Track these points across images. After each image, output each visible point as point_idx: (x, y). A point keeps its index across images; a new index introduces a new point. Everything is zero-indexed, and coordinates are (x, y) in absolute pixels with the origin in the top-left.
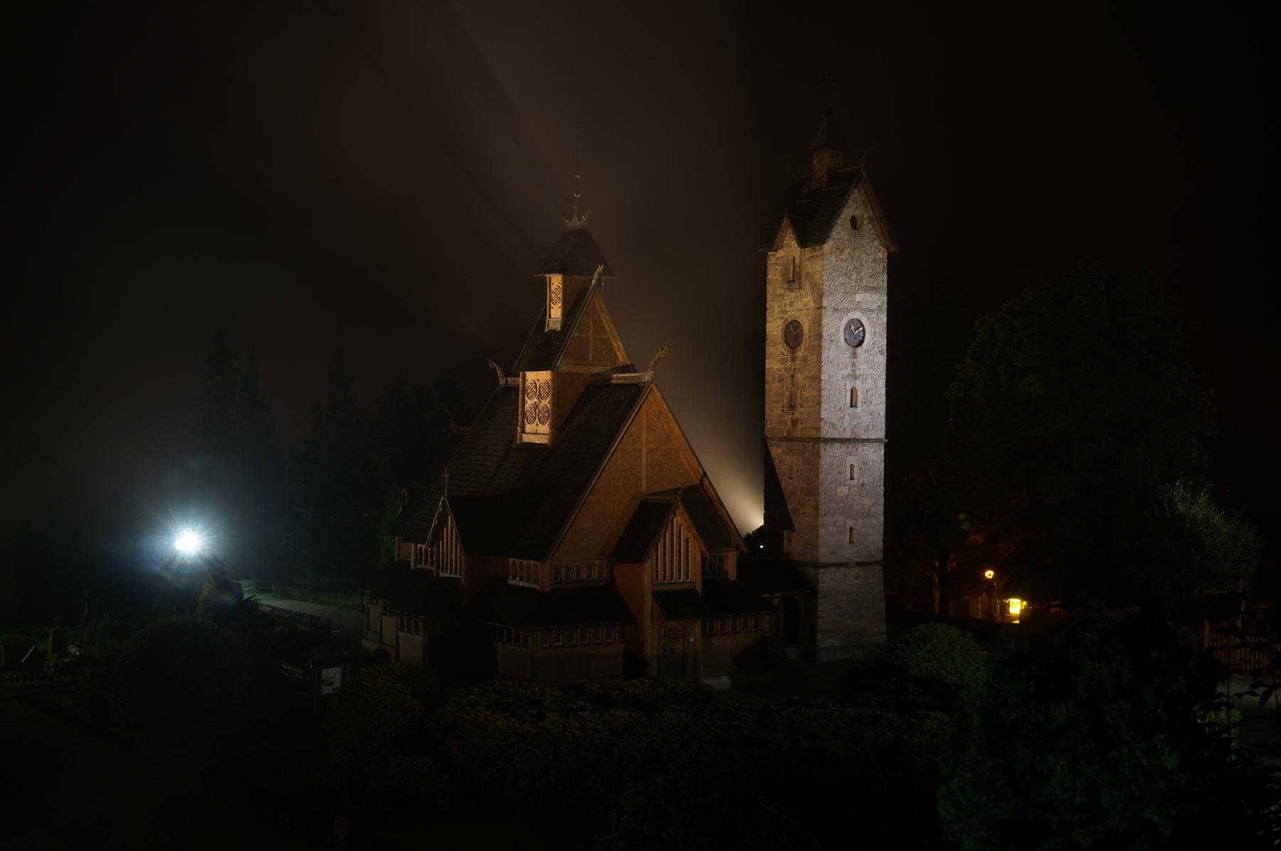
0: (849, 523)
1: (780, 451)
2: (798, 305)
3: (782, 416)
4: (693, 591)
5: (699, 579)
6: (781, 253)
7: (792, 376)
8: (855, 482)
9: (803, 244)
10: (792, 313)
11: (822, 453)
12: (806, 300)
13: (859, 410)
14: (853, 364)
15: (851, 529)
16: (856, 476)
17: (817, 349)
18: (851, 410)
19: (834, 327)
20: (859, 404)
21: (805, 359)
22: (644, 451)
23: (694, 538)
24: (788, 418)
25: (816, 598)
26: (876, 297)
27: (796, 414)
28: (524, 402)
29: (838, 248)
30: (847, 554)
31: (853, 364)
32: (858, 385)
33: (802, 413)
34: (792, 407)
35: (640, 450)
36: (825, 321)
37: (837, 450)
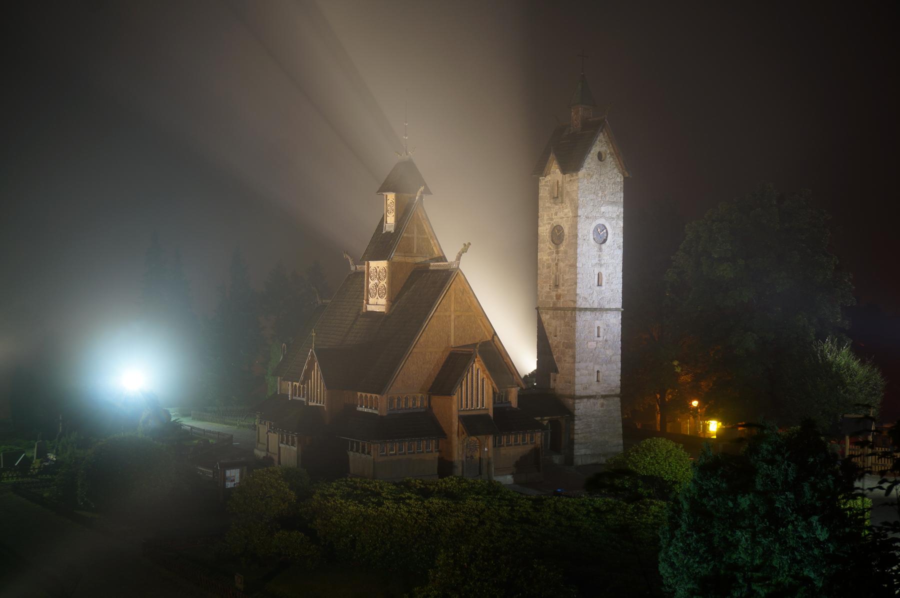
0: (597, 368)
1: (548, 317)
2: (561, 214)
3: (549, 292)
4: (487, 416)
5: (491, 407)
6: (548, 178)
7: (557, 264)
8: (601, 339)
9: (564, 171)
10: (556, 220)
11: (578, 318)
12: (566, 211)
13: (603, 288)
14: (599, 256)
15: (598, 372)
16: (601, 334)
17: (574, 245)
18: (598, 288)
19: (586, 230)
20: (604, 284)
21: (566, 252)
22: (453, 317)
23: (488, 377)
24: (554, 294)
25: (574, 420)
26: (616, 208)
27: (560, 291)
28: (368, 283)
29: (589, 175)
30: (595, 389)
31: (599, 256)
32: (603, 271)
33: (563, 290)
34: (557, 286)
35: (450, 316)
36: (580, 226)
37: (588, 316)
